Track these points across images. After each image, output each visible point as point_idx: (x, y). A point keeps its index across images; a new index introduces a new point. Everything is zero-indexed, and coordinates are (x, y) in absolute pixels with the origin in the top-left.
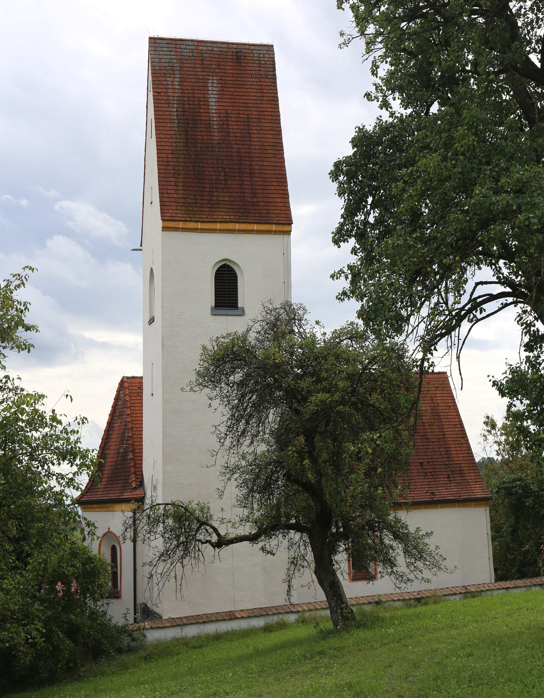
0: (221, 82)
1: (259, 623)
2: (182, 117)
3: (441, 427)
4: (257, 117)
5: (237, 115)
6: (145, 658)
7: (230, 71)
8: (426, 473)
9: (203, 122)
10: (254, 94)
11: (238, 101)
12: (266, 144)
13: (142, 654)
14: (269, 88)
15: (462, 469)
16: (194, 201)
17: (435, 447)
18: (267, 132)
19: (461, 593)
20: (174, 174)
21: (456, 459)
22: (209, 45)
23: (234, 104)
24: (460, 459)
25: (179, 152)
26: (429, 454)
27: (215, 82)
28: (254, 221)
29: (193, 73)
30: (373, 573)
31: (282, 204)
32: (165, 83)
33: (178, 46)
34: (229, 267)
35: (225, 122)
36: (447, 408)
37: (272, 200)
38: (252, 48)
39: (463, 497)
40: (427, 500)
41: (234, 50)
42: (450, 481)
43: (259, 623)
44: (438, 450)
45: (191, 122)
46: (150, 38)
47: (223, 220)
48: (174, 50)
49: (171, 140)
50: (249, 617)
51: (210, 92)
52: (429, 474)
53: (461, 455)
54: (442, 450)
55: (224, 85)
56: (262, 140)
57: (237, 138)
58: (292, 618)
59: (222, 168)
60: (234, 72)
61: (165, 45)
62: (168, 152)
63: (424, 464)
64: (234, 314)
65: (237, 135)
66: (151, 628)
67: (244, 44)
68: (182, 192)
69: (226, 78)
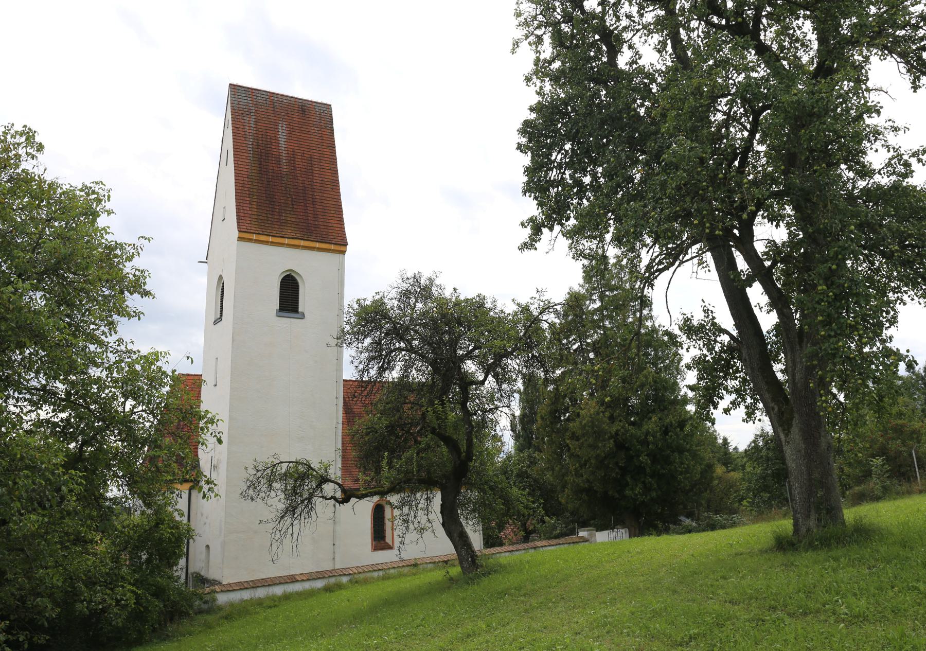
1: (319, 584)
6: (226, 618)
13: (222, 614)
30: (391, 543)
34: (293, 277)
43: (319, 584)
50: (308, 580)
58: (345, 580)
66: (222, 591)
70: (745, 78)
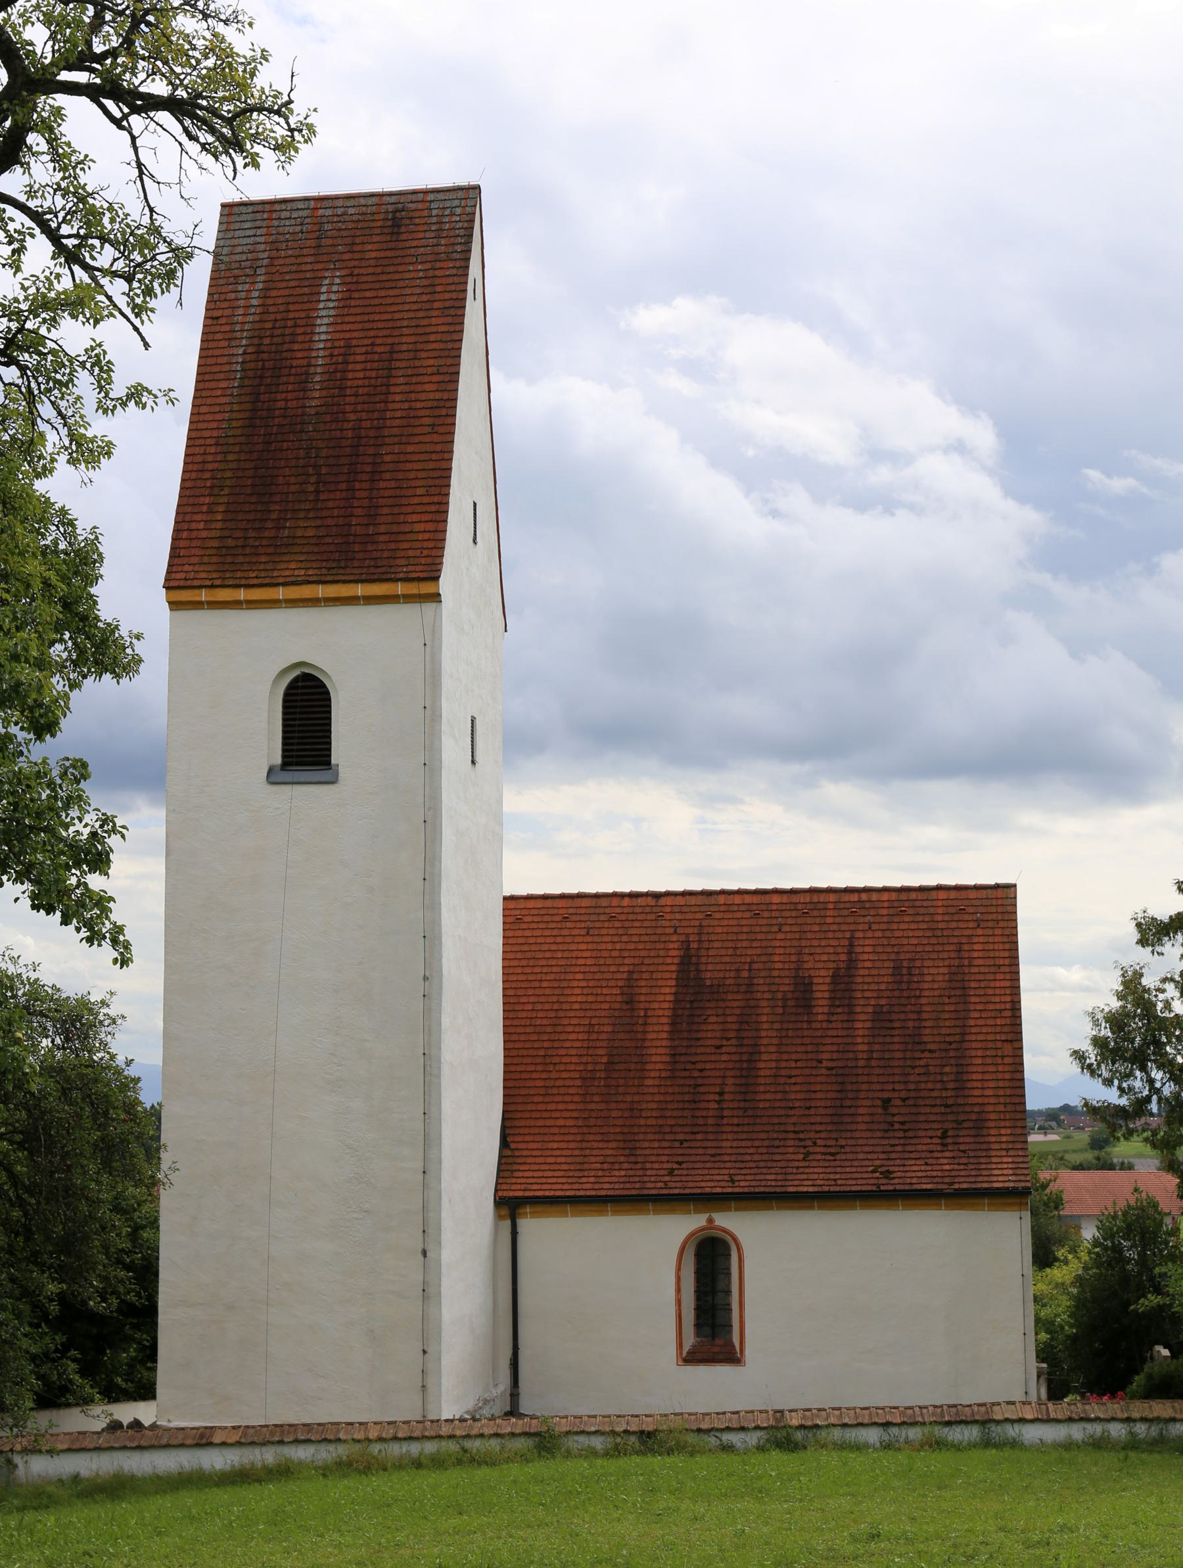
0: (349, 279)
2: (252, 365)
3: (962, 1015)
4: (411, 347)
5: (369, 348)
7: (373, 255)
8: (892, 1124)
9: (293, 371)
10: (414, 299)
11: (377, 317)
12: (419, 405)
14: (450, 280)
15: (984, 1116)
16: (240, 543)
17: (931, 1062)
18: (426, 379)
19: (757, 1428)
20: (211, 487)
21: (976, 1093)
22: (340, 203)
23: (367, 326)
24: (987, 1092)
25: (231, 441)
26: (912, 1078)
27: (337, 281)
28: (356, 577)
29: (294, 268)
31: (427, 536)
32: (233, 296)
33: (274, 215)
35: (340, 367)
36: (993, 970)
37: (407, 528)
38: (431, 197)
39: (956, 1186)
40: (864, 1188)
41: (390, 208)
42: (943, 1145)
44: (938, 1070)
45: (269, 374)
46: (223, 206)
47: (290, 579)
48: (265, 224)
49: (219, 417)
50: (239, 1444)
51: (321, 305)
52: (897, 1126)
53: (992, 1084)
54: (947, 1069)
55: (354, 287)
56: (413, 396)
57: (360, 399)
59: (314, 466)
60: (382, 254)
61: (250, 217)
62: (209, 442)
63: (894, 1102)
64: (316, 780)
65: (361, 391)
67: (415, 192)
68: (219, 525)
69: (362, 271)
70: (74, 246)
